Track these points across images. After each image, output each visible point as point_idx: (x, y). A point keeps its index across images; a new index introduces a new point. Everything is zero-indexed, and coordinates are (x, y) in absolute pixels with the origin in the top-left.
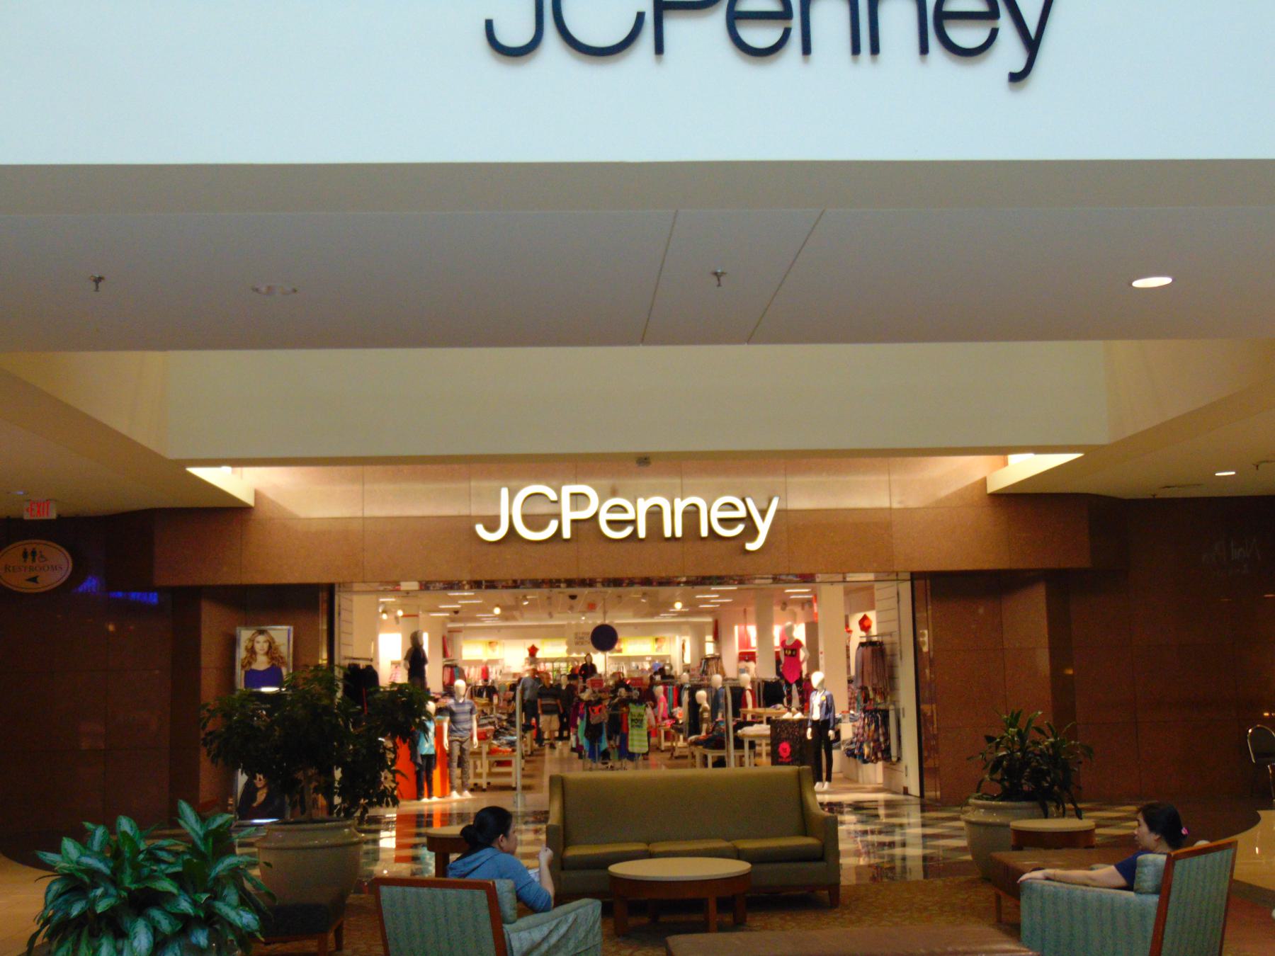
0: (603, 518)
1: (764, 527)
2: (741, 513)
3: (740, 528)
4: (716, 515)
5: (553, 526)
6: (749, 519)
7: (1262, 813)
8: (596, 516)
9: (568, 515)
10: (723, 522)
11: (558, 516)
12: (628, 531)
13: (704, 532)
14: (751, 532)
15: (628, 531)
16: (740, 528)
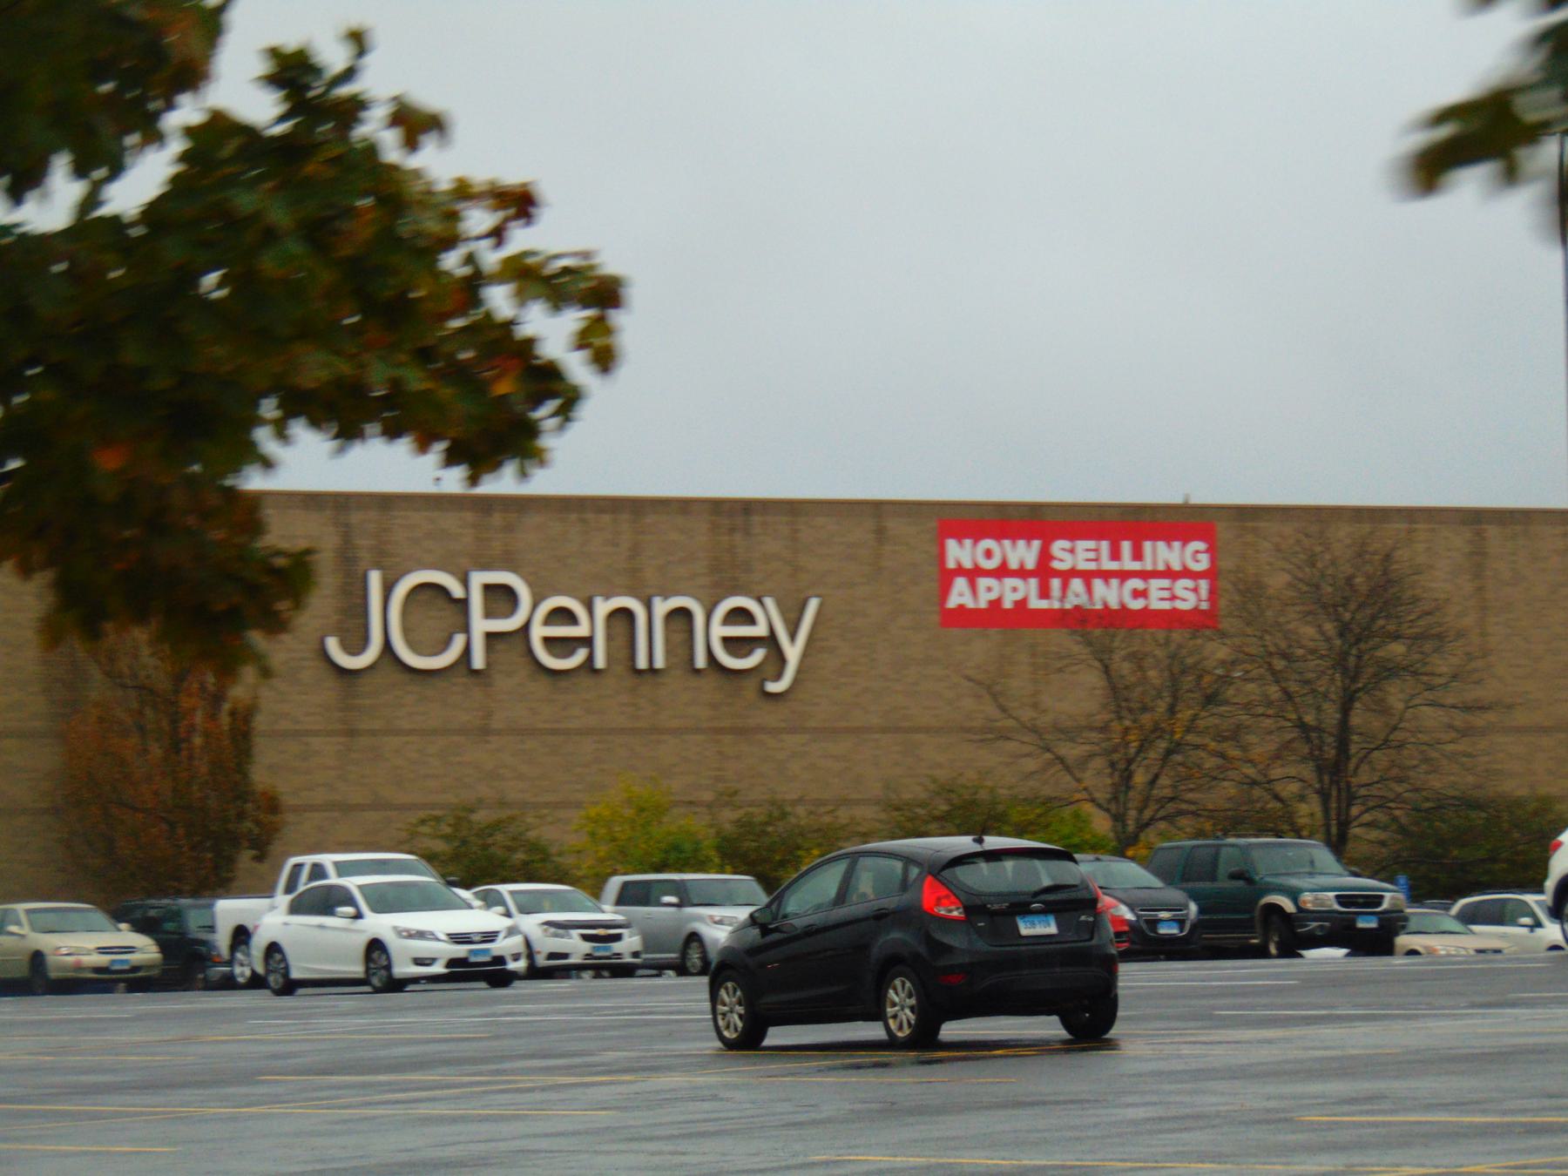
0: (538, 632)
2: (760, 630)
4: (719, 631)
5: (459, 642)
6: (771, 641)
7: (42, 579)
8: (525, 629)
9: (481, 625)
10: (728, 642)
11: (466, 629)
12: (580, 656)
13: (701, 661)
14: (777, 658)
15: (580, 656)
16: (758, 656)
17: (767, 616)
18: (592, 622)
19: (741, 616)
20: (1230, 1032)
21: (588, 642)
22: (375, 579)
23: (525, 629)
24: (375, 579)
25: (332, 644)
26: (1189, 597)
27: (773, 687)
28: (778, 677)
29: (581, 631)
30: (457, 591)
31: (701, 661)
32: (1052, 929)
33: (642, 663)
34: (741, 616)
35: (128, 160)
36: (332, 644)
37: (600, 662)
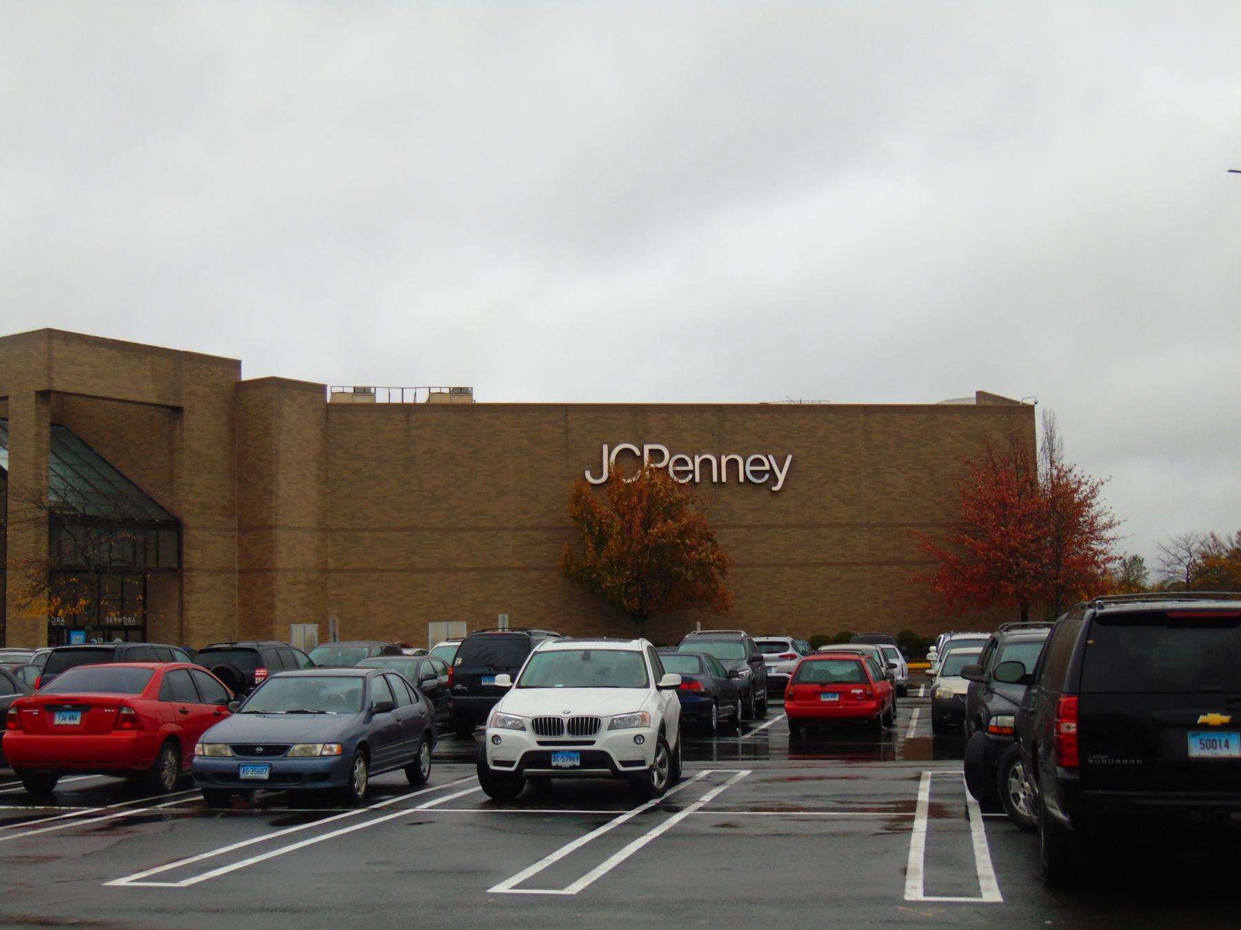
1: (781, 477)
2: (767, 467)
3: (767, 476)
4: (749, 468)
6: (771, 470)
8: (667, 467)
12: (690, 476)
13: (742, 479)
14: (774, 480)
15: (690, 476)
16: (767, 476)
17: (769, 462)
18: (695, 464)
19: (758, 462)
20: (985, 846)
21: (693, 472)
22: (605, 448)
23: (667, 467)
24: (605, 448)
25: (588, 474)
26: (507, 616)
27: (774, 489)
28: (776, 484)
29: (690, 467)
30: (638, 453)
31: (742, 479)
32: (837, 699)
33: (715, 479)
34: (758, 462)
35: (1127, 558)
36: (588, 474)
37: (697, 479)
